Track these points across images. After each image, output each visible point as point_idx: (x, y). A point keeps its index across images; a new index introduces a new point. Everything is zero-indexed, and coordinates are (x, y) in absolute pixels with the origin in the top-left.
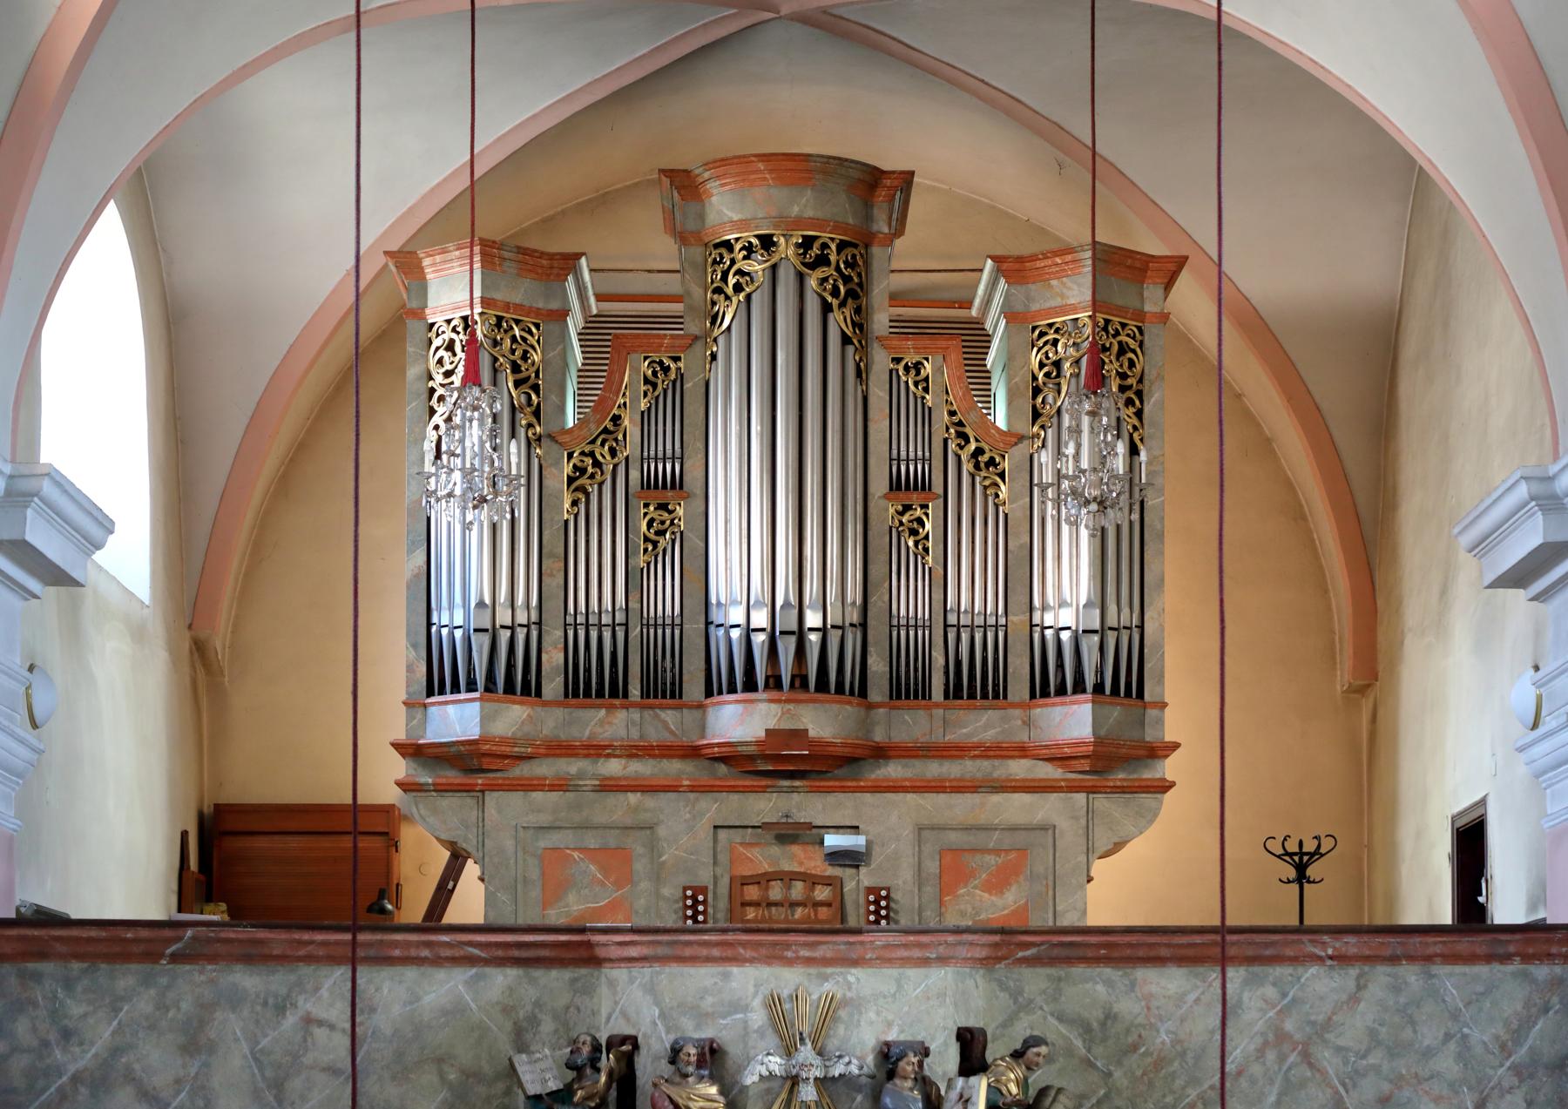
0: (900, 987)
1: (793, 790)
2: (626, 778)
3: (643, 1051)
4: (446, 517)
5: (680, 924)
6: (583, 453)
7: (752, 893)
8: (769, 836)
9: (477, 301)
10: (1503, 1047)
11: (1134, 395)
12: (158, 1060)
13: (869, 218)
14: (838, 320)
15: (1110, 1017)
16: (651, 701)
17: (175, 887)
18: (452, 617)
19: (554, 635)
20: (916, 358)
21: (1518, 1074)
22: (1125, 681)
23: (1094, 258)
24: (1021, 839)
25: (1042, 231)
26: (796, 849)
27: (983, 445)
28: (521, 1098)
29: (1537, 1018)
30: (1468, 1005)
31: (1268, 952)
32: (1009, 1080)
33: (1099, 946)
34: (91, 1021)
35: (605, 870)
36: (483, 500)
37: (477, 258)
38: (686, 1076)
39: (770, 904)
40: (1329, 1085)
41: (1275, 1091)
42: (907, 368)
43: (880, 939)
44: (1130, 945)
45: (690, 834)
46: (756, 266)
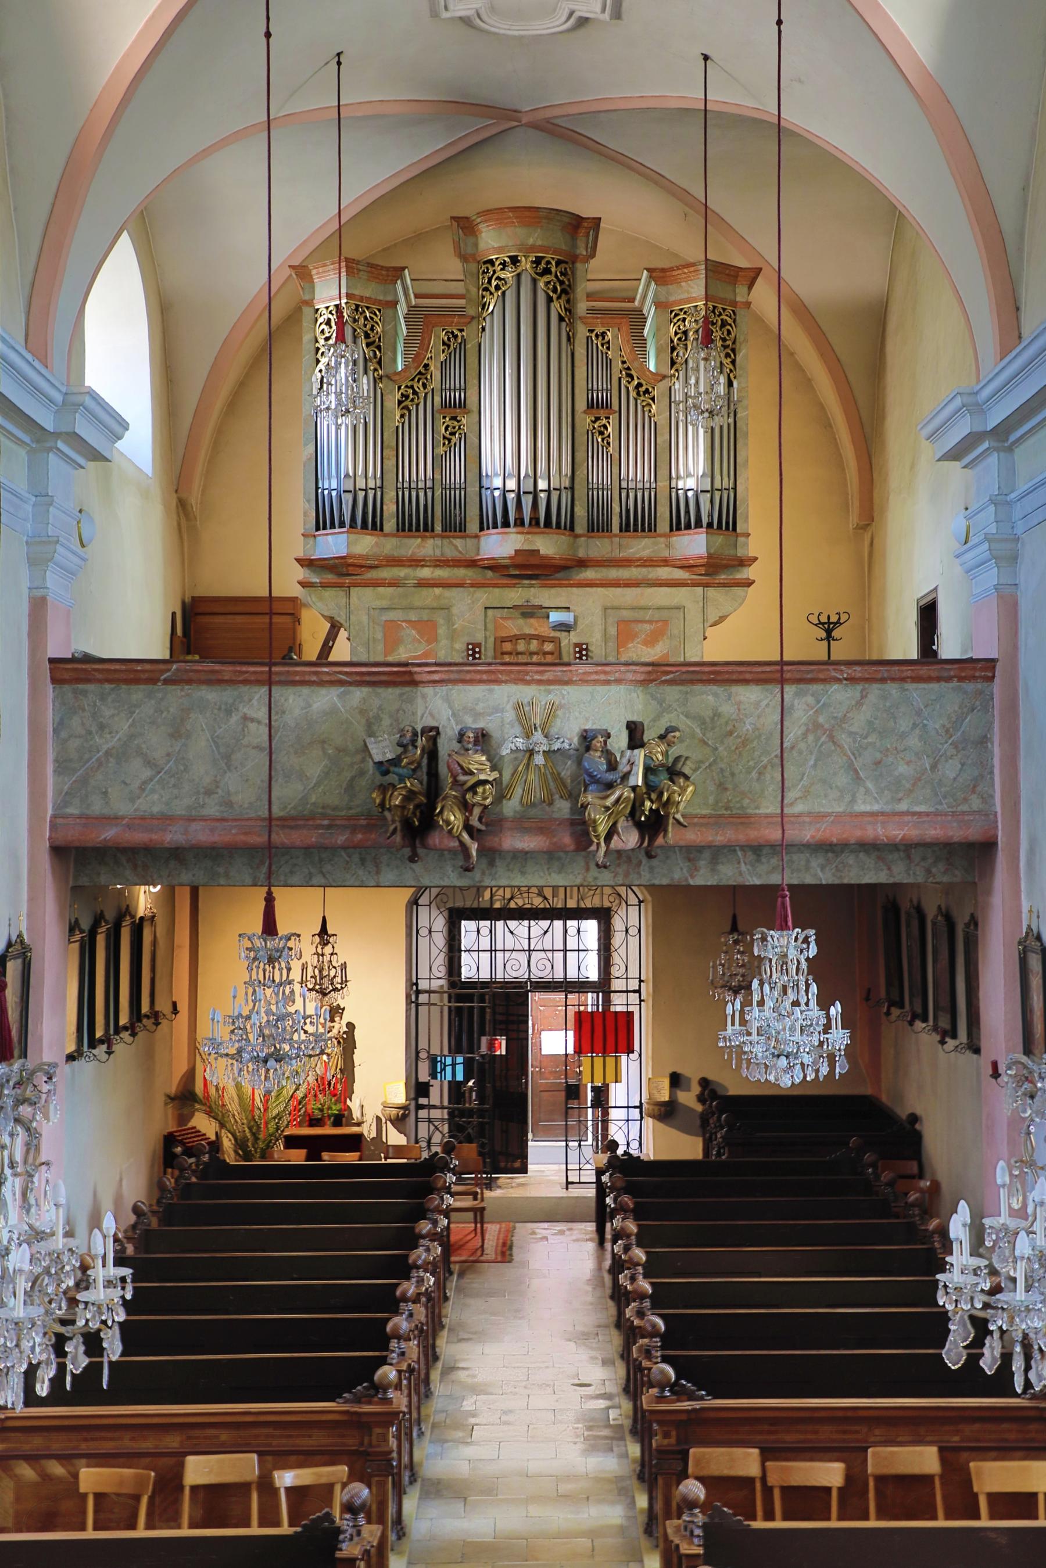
1: (531, 586)
2: (433, 579)
3: (443, 736)
4: (326, 423)
5: (465, 660)
6: (407, 387)
7: (508, 647)
8: (516, 613)
9: (343, 295)
10: (947, 731)
11: (731, 351)
12: (156, 742)
13: (574, 246)
14: (556, 305)
15: (717, 715)
16: (448, 533)
17: (168, 645)
18: (330, 483)
19: (390, 495)
21: (956, 747)
22: (726, 522)
23: (706, 269)
24: (665, 614)
25: (676, 255)
26: (532, 621)
27: (642, 381)
28: (371, 764)
29: (967, 714)
30: (926, 707)
31: (809, 676)
34: (116, 719)
35: (421, 635)
36: (347, 411)
37: (343, 270)
38: (467, 750)
39: (518, 653)
40: (845, 754)
41: (813, 757)
42: (597, 336)
43: (582, 669)
44: (727, 672)
45: (471, 614)
46: (508, 275)
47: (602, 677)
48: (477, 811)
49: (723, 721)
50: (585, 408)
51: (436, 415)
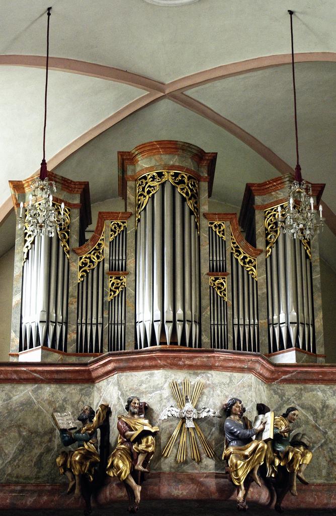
0: (231, 380)
14: (189, 204)
15: (325, 406)
20: (219, 223)
32: (282, 424)
33: (318, 373)
42: (215, 226)
47: (238, 365)
48: (141, 458)
49: (329, 411)
50: (208, 271)
51: (106, 276)
